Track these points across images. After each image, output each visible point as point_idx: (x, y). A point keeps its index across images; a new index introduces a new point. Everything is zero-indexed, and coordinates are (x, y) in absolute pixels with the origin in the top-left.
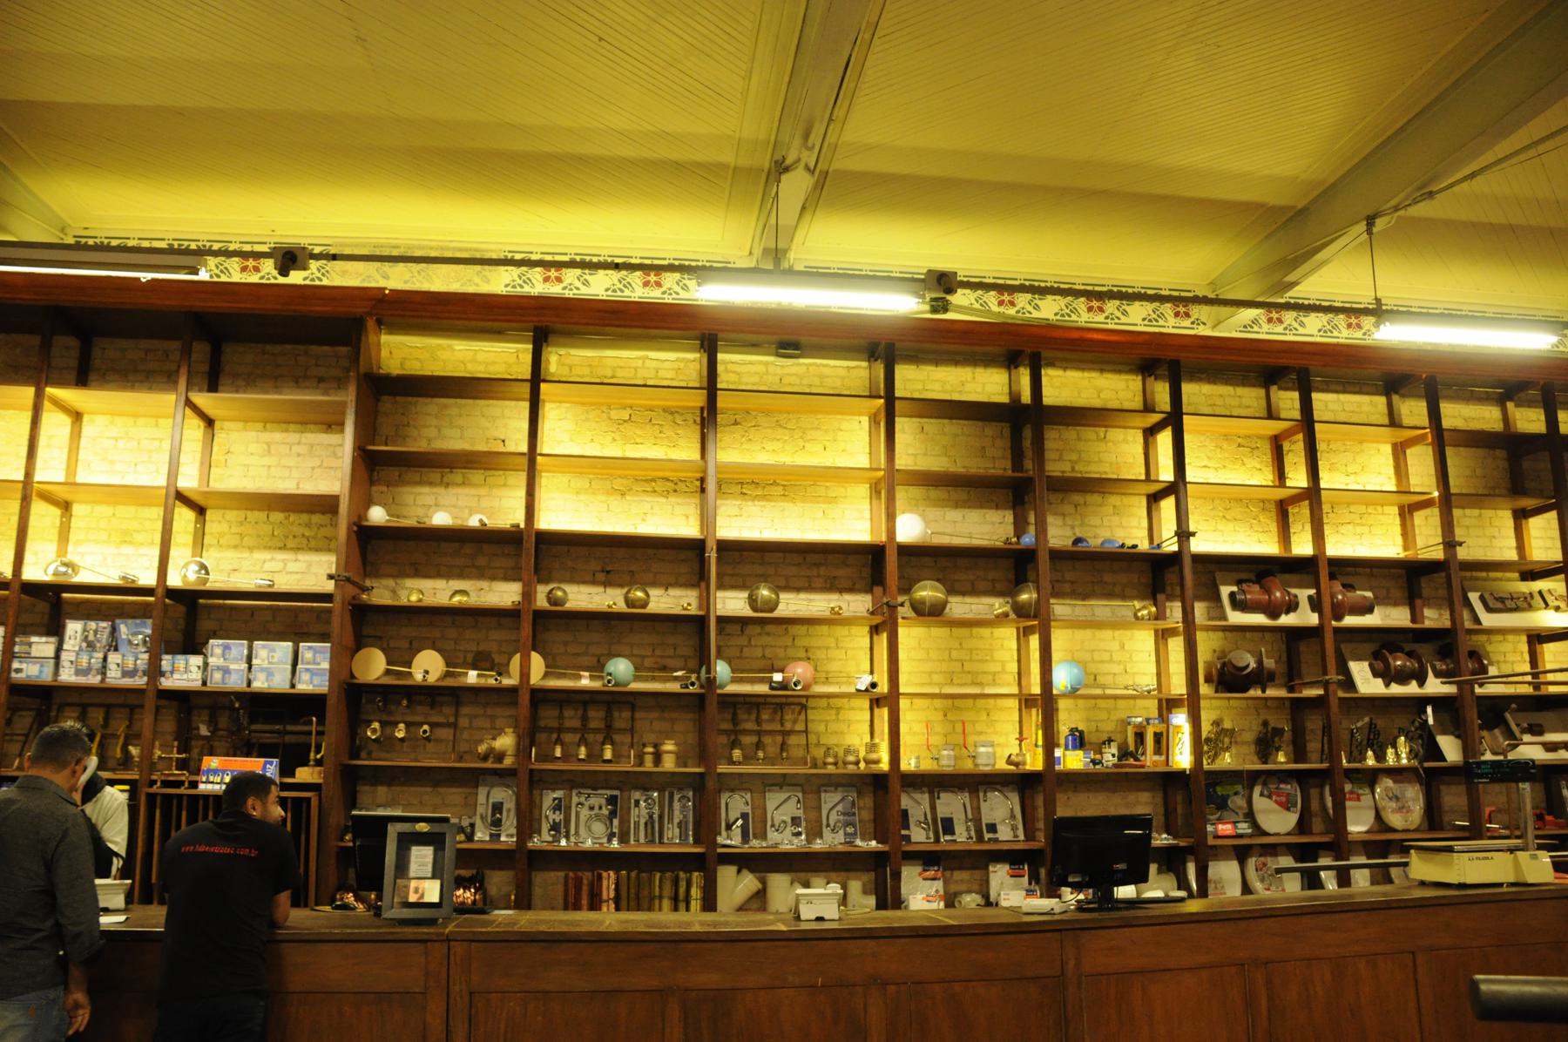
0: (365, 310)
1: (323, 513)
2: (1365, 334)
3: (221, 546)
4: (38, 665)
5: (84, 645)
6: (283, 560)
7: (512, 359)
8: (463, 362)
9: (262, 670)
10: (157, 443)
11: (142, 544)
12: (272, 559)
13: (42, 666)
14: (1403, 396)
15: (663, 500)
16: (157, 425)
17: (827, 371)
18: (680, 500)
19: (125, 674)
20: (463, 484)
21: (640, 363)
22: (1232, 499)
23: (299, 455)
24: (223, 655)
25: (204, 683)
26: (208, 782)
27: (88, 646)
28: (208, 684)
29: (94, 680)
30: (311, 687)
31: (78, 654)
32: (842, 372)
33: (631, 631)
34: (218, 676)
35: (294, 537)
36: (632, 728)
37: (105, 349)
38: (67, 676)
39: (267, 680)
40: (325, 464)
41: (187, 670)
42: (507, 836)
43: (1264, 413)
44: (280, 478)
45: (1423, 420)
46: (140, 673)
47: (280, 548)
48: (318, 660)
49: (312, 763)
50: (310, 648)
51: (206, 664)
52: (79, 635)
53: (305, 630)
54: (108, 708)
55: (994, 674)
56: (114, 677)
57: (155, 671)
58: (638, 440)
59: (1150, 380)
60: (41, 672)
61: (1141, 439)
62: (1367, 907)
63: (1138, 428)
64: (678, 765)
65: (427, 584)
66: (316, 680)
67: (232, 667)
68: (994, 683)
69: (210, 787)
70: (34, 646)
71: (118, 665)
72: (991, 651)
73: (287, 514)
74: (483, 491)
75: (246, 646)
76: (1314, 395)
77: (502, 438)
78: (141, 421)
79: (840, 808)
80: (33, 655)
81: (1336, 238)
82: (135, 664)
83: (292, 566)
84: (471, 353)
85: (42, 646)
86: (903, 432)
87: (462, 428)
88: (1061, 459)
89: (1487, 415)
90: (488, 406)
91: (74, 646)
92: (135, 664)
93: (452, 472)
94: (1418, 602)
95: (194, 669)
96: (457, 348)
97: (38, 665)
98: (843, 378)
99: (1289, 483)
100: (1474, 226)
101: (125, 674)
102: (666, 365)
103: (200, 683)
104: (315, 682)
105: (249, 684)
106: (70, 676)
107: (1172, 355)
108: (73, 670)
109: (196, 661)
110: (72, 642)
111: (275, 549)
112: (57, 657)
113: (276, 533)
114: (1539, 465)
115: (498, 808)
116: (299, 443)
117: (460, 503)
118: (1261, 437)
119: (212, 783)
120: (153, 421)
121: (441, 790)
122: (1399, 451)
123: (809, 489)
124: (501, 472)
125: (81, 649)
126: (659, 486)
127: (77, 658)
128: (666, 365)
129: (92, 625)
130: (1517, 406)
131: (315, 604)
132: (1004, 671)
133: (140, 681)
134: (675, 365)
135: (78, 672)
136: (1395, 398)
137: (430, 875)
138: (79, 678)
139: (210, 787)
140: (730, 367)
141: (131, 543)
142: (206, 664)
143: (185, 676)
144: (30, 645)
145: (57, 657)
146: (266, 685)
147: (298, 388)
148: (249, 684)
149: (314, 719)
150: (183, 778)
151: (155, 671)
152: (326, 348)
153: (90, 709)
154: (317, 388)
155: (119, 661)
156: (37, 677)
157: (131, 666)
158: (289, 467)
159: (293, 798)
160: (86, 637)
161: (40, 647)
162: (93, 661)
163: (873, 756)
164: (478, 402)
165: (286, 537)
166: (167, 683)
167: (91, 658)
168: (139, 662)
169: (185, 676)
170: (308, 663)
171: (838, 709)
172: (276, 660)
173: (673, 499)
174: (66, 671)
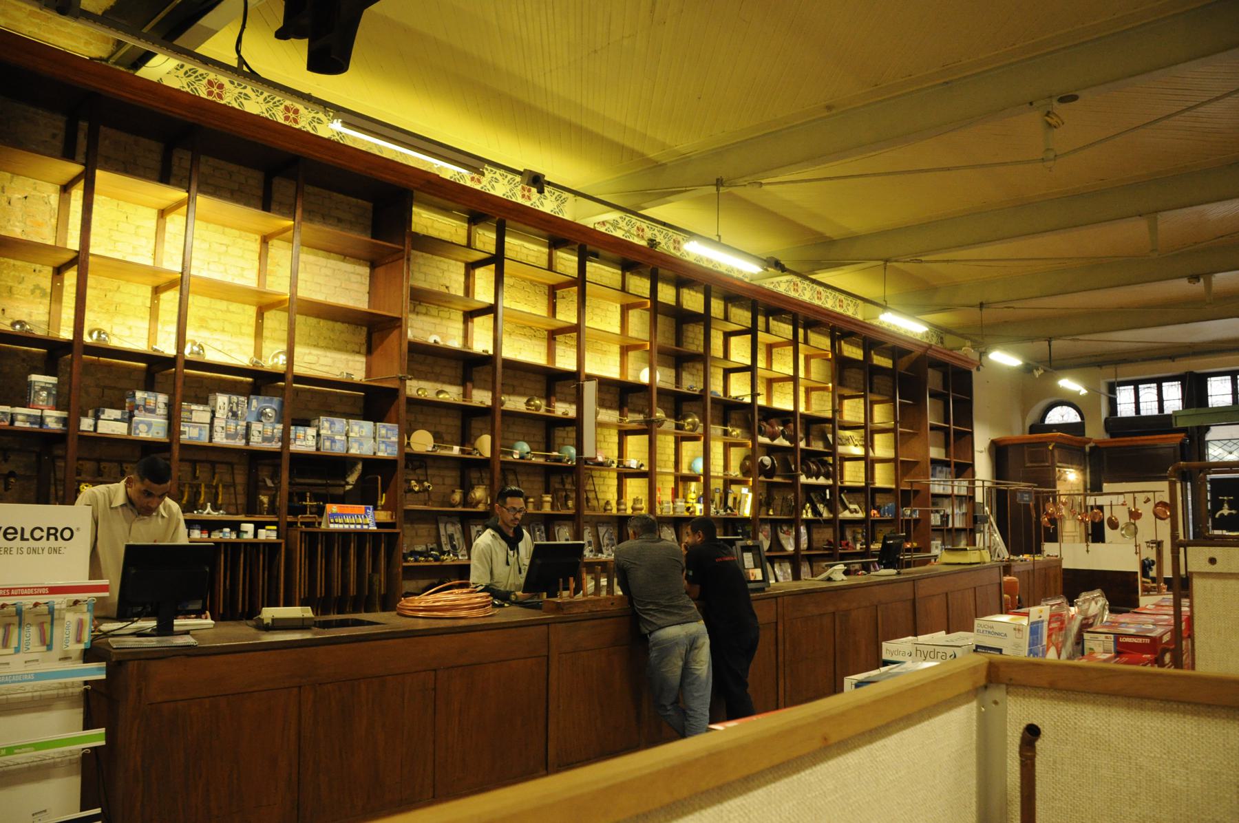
0: (415, 185)
1: (343, 322)
2: (182, 66)
3: (274, 339)
4: (198, 429)
5: (230, 414)
6: (317, 355)
7: (453, 231)
8: (426, 227)
9: (356, 441)
10: (224, 248)
11: (216, 330)
12: (310, 353)
13: (200, 430)
14: (632, 274)
15: (529, 341)
16: (223, 233)
17: (604, 273)
18: (537, 342)
19: (265, 439)
20: (426, 314)
21: (518, 249)
22: (526, 326)
23: (327, 276)
24: (330, 428)
25: (318, 449)
26: (335, 523)
27: (232, 416)
28: (322, 450)
29: (240, 443)
30: (386, 455)
31: (227, 422)
32: (610, 275)
33: (514, 424)
34: (328, 444)
35: (325, 338)
36: (234, 482)
37: (181, 158)
38: (220, 439)
39: (359, 449)
40: (343, 286)
41: (305, 438)
42: (462, 555)
43: (546, 267)
44: (314, 291)
45: (647, 293)
46: (276, 440)
47: (315, 346)
48: (389, 435)
49: (379, 508)
50: (384, 426)
51: (318, 435)
52: (226, 406)
53: (332, 409)
54: (213, 464)
55: (665, 461)
56: (256, 442)
57: (285, 438)
58: (518, 300)
59: (628, 275)
60: (200, 434)
61: (462, 271)
62: (459, 630)
63: (461, 261)
64: (534, 509)
65: (423, 384)
66: (389, 450)
67: (337, 437)
68: (665, 467)
69: (336, 526)
70: (194, 413)
71: (260, 432)
72: (665, 448)
73: (318, 320)
74: (437, 321)
75: (162, 410)
76: (588, 264)
77: (448, 285)
78: (211, 226)
79: (606, 536)
80: (193, 420)
81: (686, 191)
82: (273, 432)
83: (323, 361)
84: (431, 221)
85: (200, 414)
86: (633, 316)
87: (425, 274)
88: (693, 343)
89: (823, 342)
90: (440, 261)
91: (223, 415)
92: (273, 432)
93: (420, 304)
94: (553, 399)
95: (310, 438)
96: (424, 216)
97: (198, 429)
98: (610, 279)
99: (559, 317)
100: (622, 148)
101: (265, 439)
102: (532, 253)
103: (314, 448)
104: (389, 451)
105: (347, 451)
106: (222, 439)
107: (795, 309)
108: (224, 435)
109: (311, 432)
110: (222, 411)
111: (311, 346)
112: (212, 424)
113: (311, 334)
114: (855, 375)
115: (451, 537)
116: (326, 267)
117: (426, 328)
118: (545, 284)
119: (338, 523)
120: (220, 228)
121: (416, 526)
122: (625, 309)
123: (595, 344)
124: (447, 309)
125: (228, 417)
126: (526, 331)
127: (226, 425)
128: (532, 253)
129: (234, 398)
130: (773, 319)
131: (338, 391)
132: (669, 460)
133: (276, 446)
134: (536, 254)
135: (228, 436)
136: (730, 305)
137: (115, 615)
138: (229, 441)
139: (336, 526)
140: (562, 261)
141: (206, 328)
142: (318, 435)
143: (304, 443)
144: (191, 412)
145: (212, 424)
146: (358, 452)
147: (325, 223)
148: (347, 451)
149: (379, 478)
150: (314, 520)
151: (285, 438)
152: (341, 196)
153: (217, 466)
154: (337, 226)
155: (261, 429)
156: (197, 438)
157: (269, 434)
158: (319, 284)
159: (385, 533)
160: (232, 408)
161: (199, 413)
162: (275, 431)
163: (639, 506)
164: (435, 257)
165: (319, 338)
166: (294, 447)
167: (237, 425)
168: (238, 427)
169: (304, 443)
170: (383, 437)
171: (604, 478)
172: (364, 434)
173: (534, 342)
174: (219, 434)
